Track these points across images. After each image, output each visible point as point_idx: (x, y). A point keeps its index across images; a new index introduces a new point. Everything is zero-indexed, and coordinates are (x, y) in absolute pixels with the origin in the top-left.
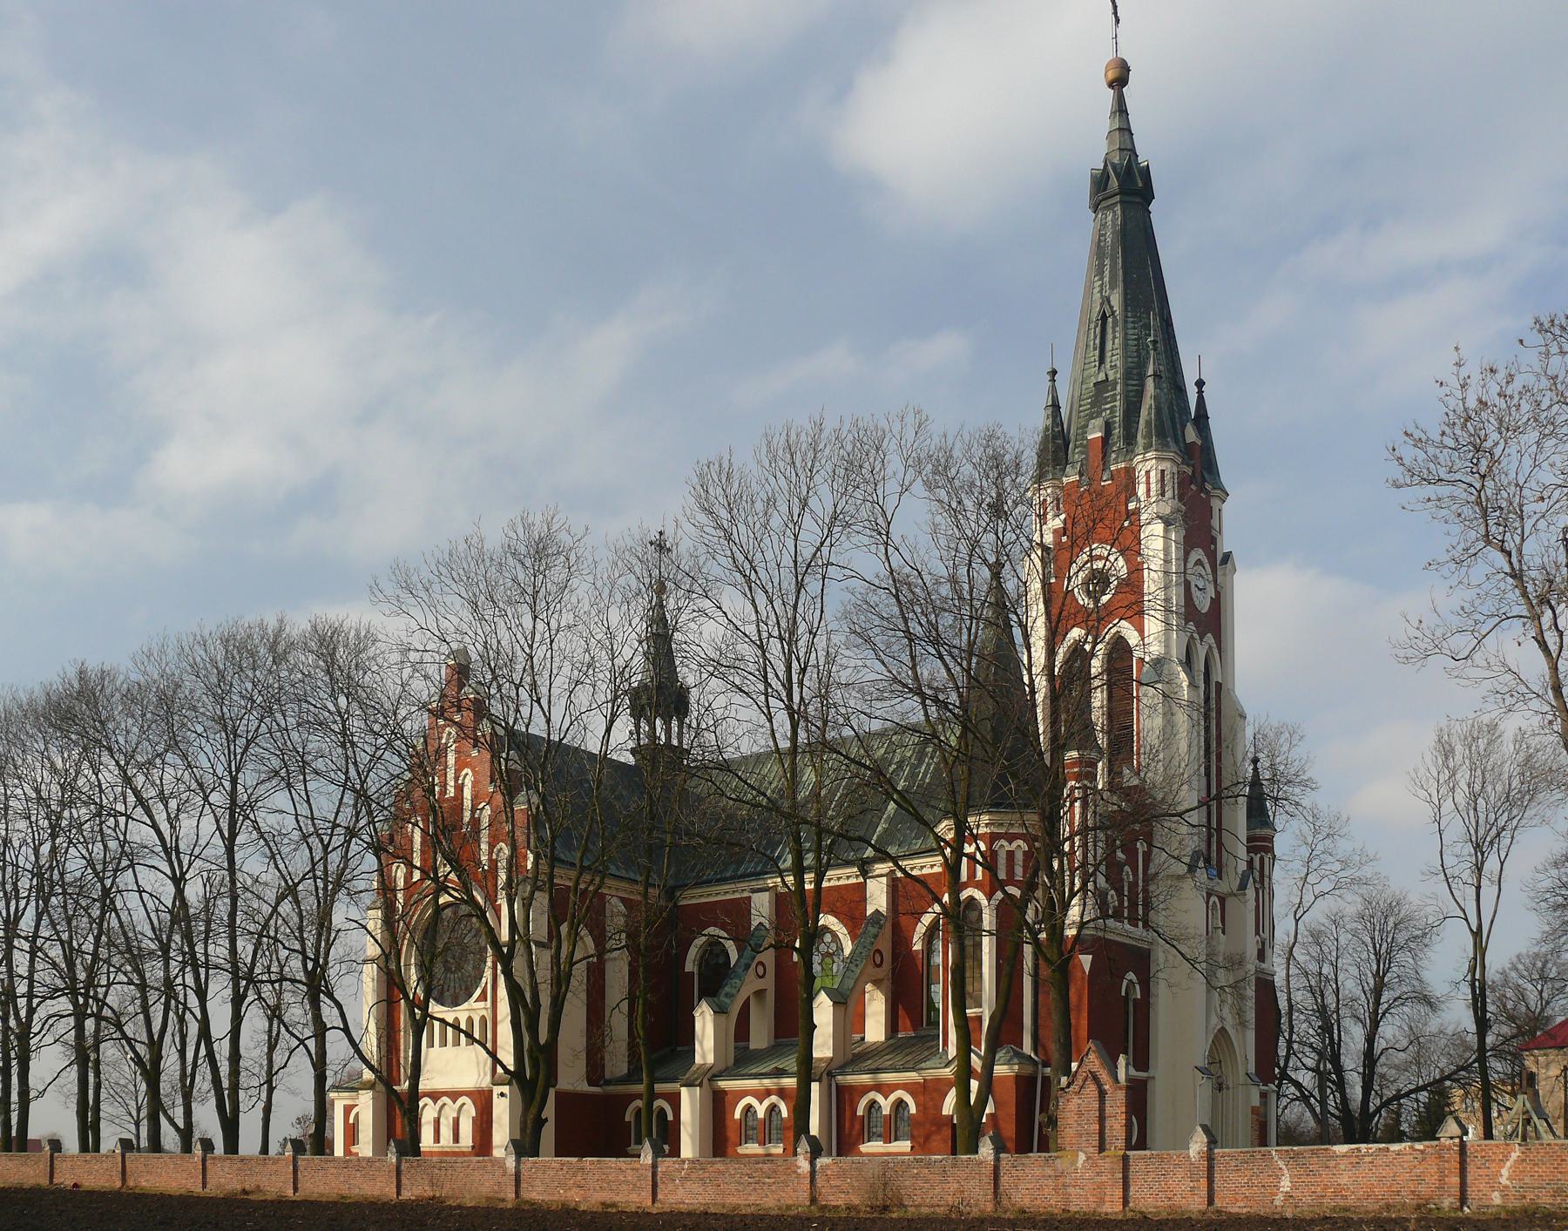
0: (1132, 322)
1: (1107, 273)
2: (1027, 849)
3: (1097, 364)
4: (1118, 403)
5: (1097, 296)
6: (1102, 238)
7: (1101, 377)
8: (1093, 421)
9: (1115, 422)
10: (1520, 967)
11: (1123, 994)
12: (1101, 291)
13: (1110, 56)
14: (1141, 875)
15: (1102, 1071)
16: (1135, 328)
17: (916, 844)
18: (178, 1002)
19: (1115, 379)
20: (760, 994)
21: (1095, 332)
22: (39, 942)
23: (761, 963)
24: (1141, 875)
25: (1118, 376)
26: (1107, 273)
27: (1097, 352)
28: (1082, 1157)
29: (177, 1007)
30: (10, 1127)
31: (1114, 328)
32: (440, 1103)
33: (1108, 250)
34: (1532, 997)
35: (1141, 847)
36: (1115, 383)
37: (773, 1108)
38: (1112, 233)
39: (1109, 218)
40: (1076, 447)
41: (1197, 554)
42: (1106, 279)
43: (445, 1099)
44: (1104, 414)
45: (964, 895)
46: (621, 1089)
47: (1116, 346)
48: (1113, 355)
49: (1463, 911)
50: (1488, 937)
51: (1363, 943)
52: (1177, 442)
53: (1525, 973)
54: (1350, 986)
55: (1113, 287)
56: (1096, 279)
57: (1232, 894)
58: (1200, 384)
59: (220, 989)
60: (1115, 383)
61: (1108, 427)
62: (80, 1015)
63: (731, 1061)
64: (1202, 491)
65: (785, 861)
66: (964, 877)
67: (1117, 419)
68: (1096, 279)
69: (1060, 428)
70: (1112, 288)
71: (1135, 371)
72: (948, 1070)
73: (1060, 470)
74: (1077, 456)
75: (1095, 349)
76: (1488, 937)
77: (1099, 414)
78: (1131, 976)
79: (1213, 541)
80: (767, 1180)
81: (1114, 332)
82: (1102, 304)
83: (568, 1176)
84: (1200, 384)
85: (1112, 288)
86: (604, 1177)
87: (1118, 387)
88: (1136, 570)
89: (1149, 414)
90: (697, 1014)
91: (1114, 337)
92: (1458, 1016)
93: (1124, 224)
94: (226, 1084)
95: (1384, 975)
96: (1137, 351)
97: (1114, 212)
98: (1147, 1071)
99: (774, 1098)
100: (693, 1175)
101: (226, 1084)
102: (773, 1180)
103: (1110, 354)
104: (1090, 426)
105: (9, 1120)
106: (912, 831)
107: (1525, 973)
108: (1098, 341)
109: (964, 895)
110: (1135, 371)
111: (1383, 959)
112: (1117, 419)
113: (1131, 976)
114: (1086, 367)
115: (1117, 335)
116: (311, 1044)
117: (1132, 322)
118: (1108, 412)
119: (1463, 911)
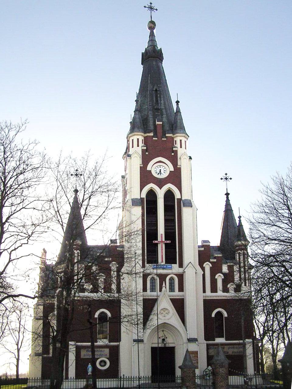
58: (177, 102)
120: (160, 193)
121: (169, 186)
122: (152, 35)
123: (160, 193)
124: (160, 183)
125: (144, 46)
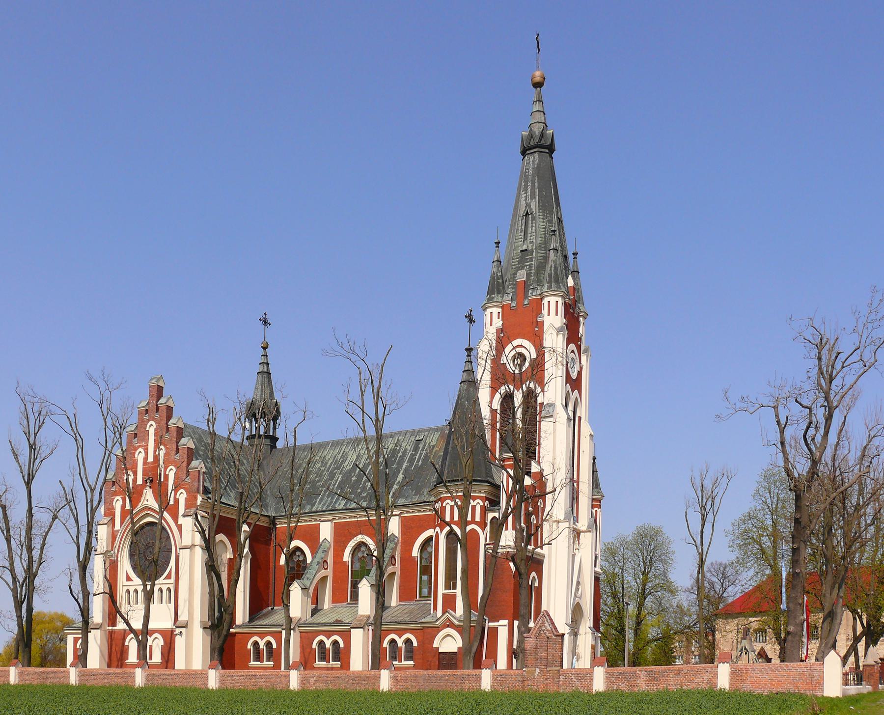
0: (543, 219)
1: (529, 190)
2: (482, 505)
3: (522, 240)
4: (533, 263)
5: (523, 203)
6: (527, 171)
7: (524, 247)
8: (519, 271)
9: (531, 273)
10: (712, 570)
11: (530, 584)
12: (526, 200)
15: (839, 606)
16: (543, 222)
17: (415, 499)
19: (532, 249)
21: (522, 222)
25: (534, 248)
26: (529, 190)
27: (523, 234)
31: (532, 221)
33: (530, 178)
34: (718, 587)
36: (532, 251)
37: (408, 642)
38: (533, 168)
39: (531, 160)
40: (510, 285)
41: (572, 346)
42: (529, 194)
44: (525, 268)
45: (468, 528)
47: (533, 231)
48: (531, 236)
49: (695, 542)
50: (707, 554)
51: (637, 555)
53: (715, 574)
54: (629, 578)
55: (532, 197)
56: (523, 192)
57: (583, 532)
60: (532, 251)
61: (529, 275)
63: (247, 620)
65: (339, 504)
66: (469, 519)
67: (533, 271)
68: (523, 192)
69: (501, 274)
70: (532, 199)
71: (543, 246)
72: (457, 623)
73: (501, 297)
74: (510, 289)
75: (521, 232)
76: (707, 554)
77: (523, 268)
78: (533, 574)
80: (364, 682)
81: (532, 223)
82: (526, 207)
83: (246, 680)
85: (532, 199)
86: (268, 680)
87: (534, 254)
89: (551, 270)
91: (532, 226)
92: (686, 599)
93: (539, 164)
95: (648, 574)
96: (545, 234)
97: (534, 158)
100: (321, 679)
102: (367, 682)
103: (530, 235)
104: (518, 274)
105: (804, 601)
106: (412, 491)
107: (715, 574)
108: (523, 227)
109: (468, 528)
110: (543, 246)
111: (649, 564)
112: (533, 271)
113: (533, 574)
114: (517, 241)
115: (534, 225)
117: (543, 219)
118: (528, 267)
119: (695, 542)
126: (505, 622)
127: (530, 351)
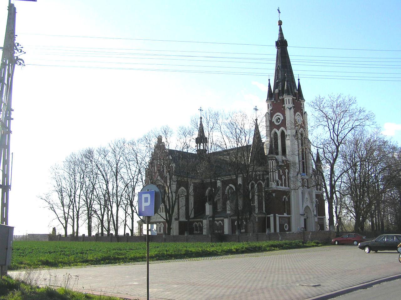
13: (279, 20)
14: (287, 177)
18: (129, 200)
20: (219, 200)
22: (80, 196)
23: (219, 194)
24: (287, 177)
28: (251, 234)
29: (130, 199)
30: (170, 206)
32: (161, 224)
35: (287, 170)
41: (298, 113)
43: (158, 223)
46: (192, 220)
52: (292, 92)
58: (299, 80)
59: (114, 205)
62: (88, 210)
64: (298, 101)
79: (302, 110)
84: (299, 80)
88: (285, 117)
90: (206, 205)
94: (116, 223)
98: (290, 215)
99: (220, 222)
101: (116, 223)
116: (131, 215)
120: (279, 133)
121: (282, 128)
122: (281, 30)
123: (279, 133)
124: (278, 127)
125: (276, 38)
126: (272, 215)
127: (282, 118)
